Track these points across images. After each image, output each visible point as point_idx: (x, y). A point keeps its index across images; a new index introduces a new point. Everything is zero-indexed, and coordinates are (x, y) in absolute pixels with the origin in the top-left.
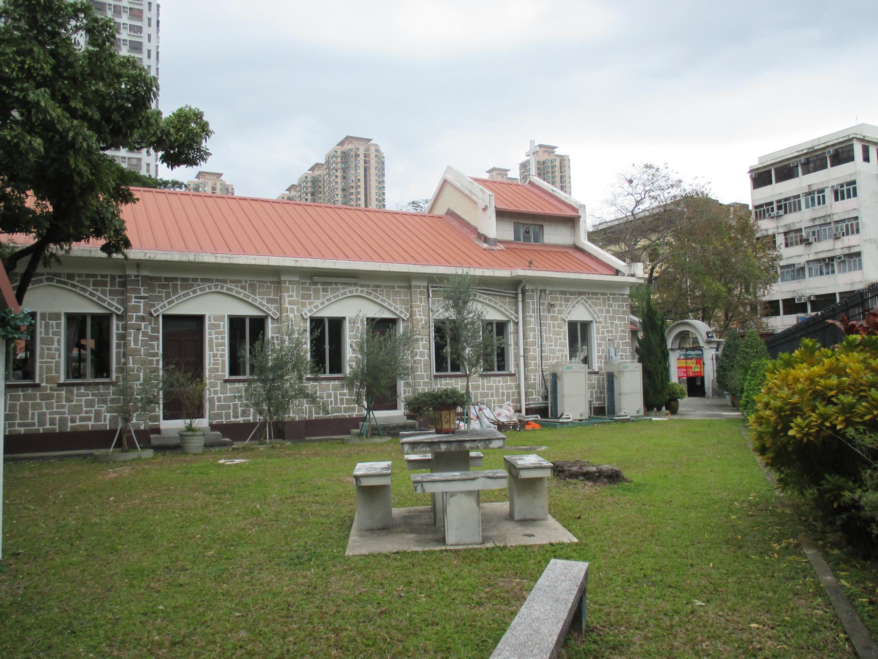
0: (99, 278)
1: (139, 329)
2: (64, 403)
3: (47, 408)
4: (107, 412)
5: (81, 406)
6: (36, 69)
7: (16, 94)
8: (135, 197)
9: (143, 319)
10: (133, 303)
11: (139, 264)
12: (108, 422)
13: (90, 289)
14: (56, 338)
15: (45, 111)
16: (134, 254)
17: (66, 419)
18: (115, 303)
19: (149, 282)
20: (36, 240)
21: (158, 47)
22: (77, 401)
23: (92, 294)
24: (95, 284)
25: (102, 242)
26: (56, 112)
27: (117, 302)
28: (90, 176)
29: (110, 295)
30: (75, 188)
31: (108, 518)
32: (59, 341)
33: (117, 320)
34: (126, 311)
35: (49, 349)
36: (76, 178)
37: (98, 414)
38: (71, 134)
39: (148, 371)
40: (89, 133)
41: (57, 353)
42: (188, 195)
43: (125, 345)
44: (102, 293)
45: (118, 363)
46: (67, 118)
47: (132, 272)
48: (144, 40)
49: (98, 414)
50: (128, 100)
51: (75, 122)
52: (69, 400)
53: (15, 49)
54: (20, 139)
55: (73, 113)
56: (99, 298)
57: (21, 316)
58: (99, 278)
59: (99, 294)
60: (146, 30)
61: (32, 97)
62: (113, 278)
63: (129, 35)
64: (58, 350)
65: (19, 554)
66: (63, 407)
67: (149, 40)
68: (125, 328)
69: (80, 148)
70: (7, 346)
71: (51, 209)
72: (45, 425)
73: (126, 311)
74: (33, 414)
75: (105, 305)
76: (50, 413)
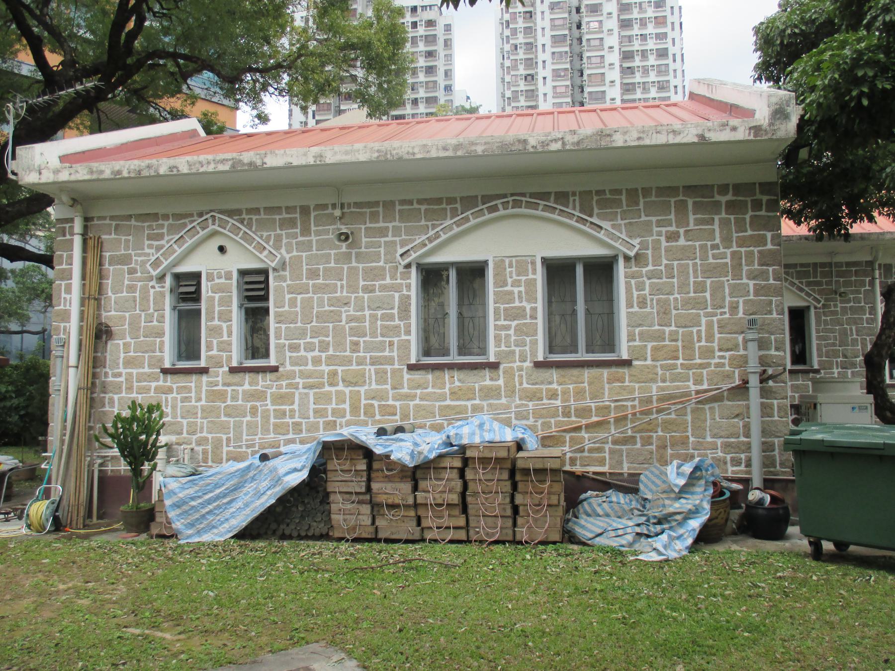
42: (615, 109)
48: (669, 45)
60: (671, 35)
63: (655, 44)
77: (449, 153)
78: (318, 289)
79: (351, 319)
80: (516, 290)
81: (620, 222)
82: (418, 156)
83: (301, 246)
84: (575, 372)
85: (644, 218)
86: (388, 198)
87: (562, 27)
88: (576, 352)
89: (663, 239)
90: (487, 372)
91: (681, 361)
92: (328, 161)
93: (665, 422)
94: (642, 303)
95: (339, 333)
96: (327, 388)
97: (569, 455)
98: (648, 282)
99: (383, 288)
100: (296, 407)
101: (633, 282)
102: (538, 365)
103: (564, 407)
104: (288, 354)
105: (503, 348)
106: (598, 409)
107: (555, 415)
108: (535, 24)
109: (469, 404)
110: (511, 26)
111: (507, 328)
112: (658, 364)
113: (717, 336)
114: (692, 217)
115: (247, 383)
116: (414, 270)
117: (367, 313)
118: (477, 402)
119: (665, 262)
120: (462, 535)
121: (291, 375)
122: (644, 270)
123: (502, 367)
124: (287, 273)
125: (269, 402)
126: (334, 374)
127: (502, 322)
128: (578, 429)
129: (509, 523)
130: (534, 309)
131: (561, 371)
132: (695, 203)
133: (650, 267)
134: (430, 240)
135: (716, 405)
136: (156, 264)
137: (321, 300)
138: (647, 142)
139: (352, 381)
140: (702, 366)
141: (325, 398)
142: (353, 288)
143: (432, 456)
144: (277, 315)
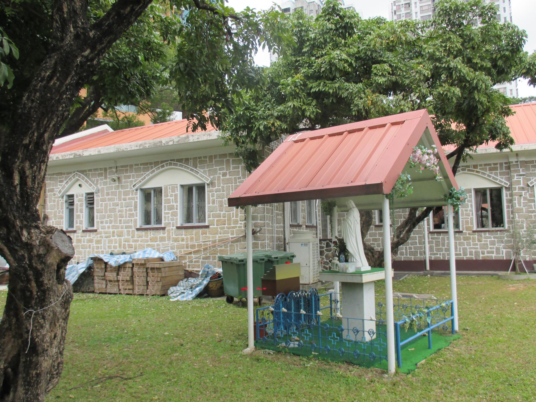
0: (492, 166)
1: (521, 196)
2: (477, 242)
3: (467, 245)
4: (504, 248)
5: (487, 244)
6: (453, 48)
7: (444, 65)
8: (513, 111)
9: (523, 189)
10: (515, 179)
11: (517, 154)
12: (504, 255)
13: (488, 173)
14: (470, 204)
15: (460, 71)
16: (515, 148)
17: (479, 252)
18: (503, 180)
19: (525, 164)
20: (456, 148)
21: (511, 13)
22: (484, 241)
23: (489, 176)
24: (490, 170)
25: (496, 142)
26: (465, 70)
27: (505, 179)
28: (487, 104)
29: (500, 175)
30: (479, 112)
31: (516, 316)
32: (471, 205)
33: (506, 191)
34: (511, 185)
35: (466, 211)
36: (479, 106)
37: (498, 250)
38: (475, 81)
39: (529, 222)
40: (486, 78)
41: (471, 213)
43: (512, 206)
44: (495, 175)
45: (509, 217)
46: (472, 72)
47: (513, 160)
49: (498, 250)
50: (507, 50)
51: (477, 73)
52: (480, 241)
53: (441, 40)
54: (447, 91)
55: (475, 67)
56: (493, 178)
57: (460, 192)
58: (492, 166)
59: (493, 175)
61: (452, 64)
62: (501, 164)
64: (472, 211)
65: (467, 330)
66: (476, 244)
67: (505, 11)
68: (511, 195)
69: (481, 88)
70: (454, 209)
71: (464, 128)
72: (467, 255)
73: (511, 185)
74: (460, 248)
75: (498, 182)
76: (470, 248)
77: (138, 148)
78: (110, 200)
79: (119, 211)
80: (171, 198)
81: (206, 169)
82: (129, 149)
83: (105, 183)
84: (190, 230)
85: (214, 167)
86: (131, 164)
87: (428, 10)
88: (192, 222)
89: (221, 176)
90: (161, 231)
91: (226, 226)
92: (102, 153)
93: (220, 250)
94: (213, 202)
95: (115, 216)
96: (112, 238)
97: (188, 263)
98: (215, 193)
99: (129, 199)
100: (102, 245)
101: (210, 193)
102: (178, 228)
103: (187, 244)
104: (100, 225)
105: (167, 221)
106: (198, 245)
107: (183, 248)
108: (411, 10)
109: (156, 243)
110: (397, 13)
111: (168, 213)
112: (218, 227)
113: (239, 215)
114: (231, 166)
115: (89, 236)
116: (139, 191)
117: (124, 208)
118: (158, 243)
119: (222, 185)
120: (131, 292)
121: (101, 233)
122: (214, 189)
123: (166, 229)
124: (100, 194)
125: (94, 243)
126: (114, 232)
127: (167, 211)
128: (190, 253)
129: (146, 287)
130: (177, 206)
131: (186, 230)
132: (233, 160)
133: (216, 188)
134: (142, 179)
135: (238, 243)
136: (60, 192)
137: (110, 204)
138: (200, 140)
139: (120, 235)
140: (233, 227)
141: (110, 242)
142: (120, 199)
143: (122, 263)
144: (97, 210)
